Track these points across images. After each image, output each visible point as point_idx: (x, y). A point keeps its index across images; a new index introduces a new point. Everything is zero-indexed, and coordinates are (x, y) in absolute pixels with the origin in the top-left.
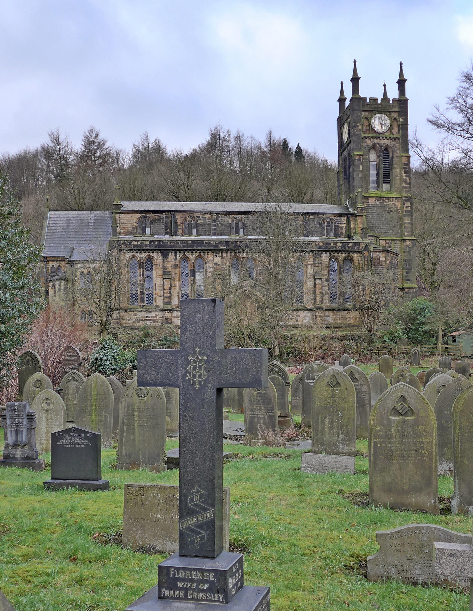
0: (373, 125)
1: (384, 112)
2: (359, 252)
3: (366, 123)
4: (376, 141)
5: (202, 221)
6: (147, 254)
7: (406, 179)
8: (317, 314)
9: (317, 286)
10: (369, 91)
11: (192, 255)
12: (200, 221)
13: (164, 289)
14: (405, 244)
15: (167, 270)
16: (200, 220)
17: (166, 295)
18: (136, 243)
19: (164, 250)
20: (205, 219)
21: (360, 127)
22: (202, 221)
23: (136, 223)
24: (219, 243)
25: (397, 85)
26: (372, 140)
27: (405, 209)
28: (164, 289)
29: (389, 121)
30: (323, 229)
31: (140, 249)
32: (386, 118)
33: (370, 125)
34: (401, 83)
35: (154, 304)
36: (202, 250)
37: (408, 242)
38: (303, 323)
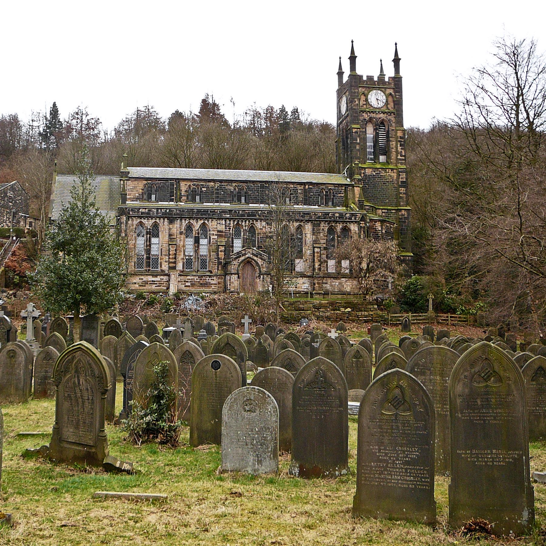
0: (369, 100)
1: (379, 89)
2: (356, 222)
3: (363, 98)
4: (372, 115)
5: (205, 189)
6: (154, 221)
7: (401, 152)
8: (316, 281)
9: (316, 254)
10: (367, 69)
11: (197, 222)
12: (203, 189)
13: (169, 255)
14: (400, 213)
15: (173, 237)
16: (204, 187)
17: (171, 260)
18: (144, 211)
19: (171, 217)
20: (208, 187)
21: (357, 102)
22: (205, 189)
23: (142, 189)
24: (222, 212)
25: (393, 63)
26: (369, 114)
27: (400, 180)
28: (169, 255)
29: (384, 97)
30: (322, 198)
31: (148, 216)
32: (382, 94)
33: (367, 100)
34: (396, 61)
35: (159, 269)
36: (206, 218)
37: (403, 212)
38: (302, 290)
